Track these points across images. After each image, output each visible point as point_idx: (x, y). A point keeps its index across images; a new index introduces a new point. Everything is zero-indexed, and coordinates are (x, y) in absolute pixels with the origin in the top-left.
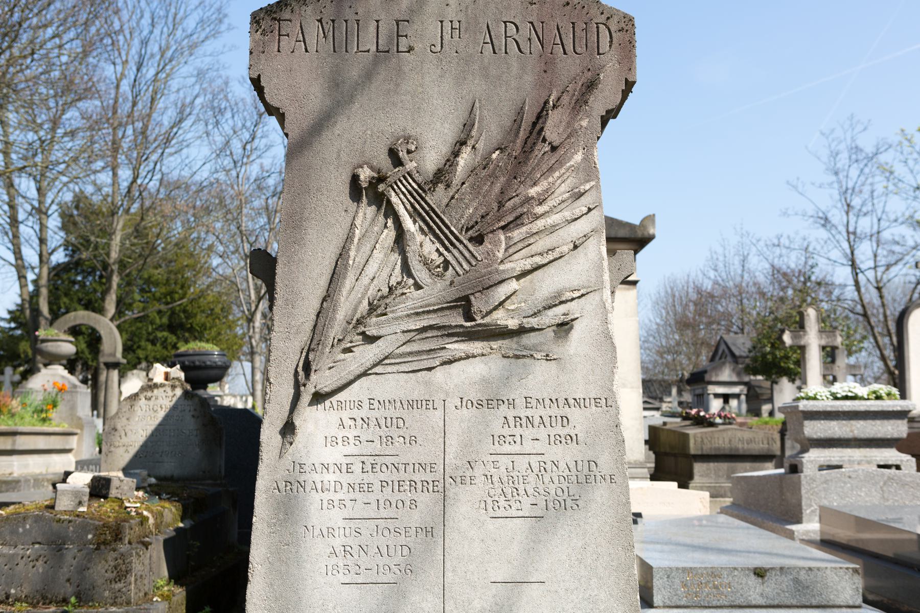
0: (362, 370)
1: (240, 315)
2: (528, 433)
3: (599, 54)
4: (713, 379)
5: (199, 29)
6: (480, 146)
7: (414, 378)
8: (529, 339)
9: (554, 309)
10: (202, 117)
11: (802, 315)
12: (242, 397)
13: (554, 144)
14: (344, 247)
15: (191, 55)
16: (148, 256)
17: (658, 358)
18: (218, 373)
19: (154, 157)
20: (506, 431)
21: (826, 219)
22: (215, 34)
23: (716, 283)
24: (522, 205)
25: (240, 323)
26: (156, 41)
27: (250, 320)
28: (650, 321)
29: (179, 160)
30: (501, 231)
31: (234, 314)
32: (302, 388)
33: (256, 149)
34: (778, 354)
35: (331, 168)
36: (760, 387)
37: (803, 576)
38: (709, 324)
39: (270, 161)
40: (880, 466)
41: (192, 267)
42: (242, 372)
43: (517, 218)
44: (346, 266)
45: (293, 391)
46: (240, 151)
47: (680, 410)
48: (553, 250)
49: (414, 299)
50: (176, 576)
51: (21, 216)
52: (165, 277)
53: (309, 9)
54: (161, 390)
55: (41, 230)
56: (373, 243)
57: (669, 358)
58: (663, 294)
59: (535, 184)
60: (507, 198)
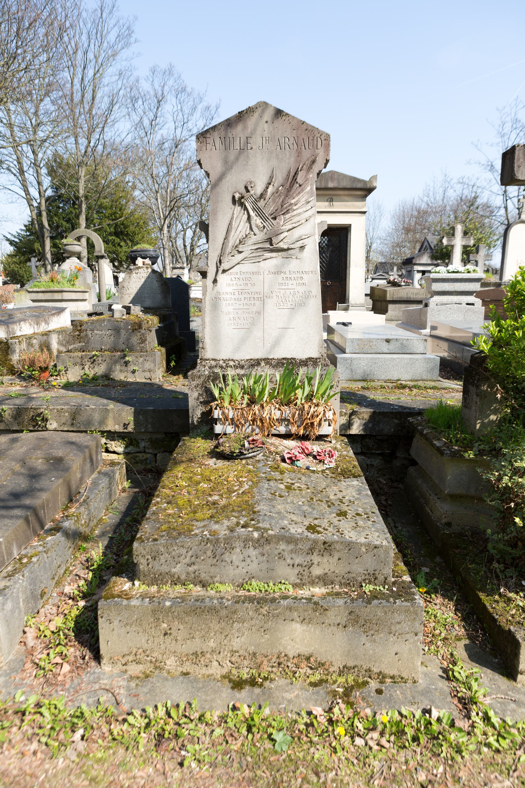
2: (290, 282)
4: (417, 262)
8: (290, 252)
11: (453, 229)
20: (283, 282)
21: (492, 166)
22: (127, 45)
27: (161, 230)
37: (404, 342)
39: (166, 131)
40: (467, 304)
41: (125, 197)
44: (231, 228)
49: (254, 239)
50: (161, 343)
51: (25, 169)
55: (38, 176)
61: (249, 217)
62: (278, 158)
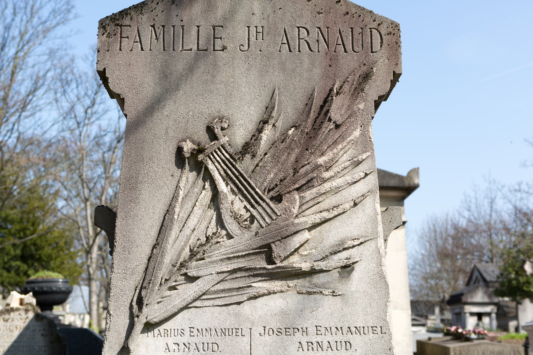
0: (184, 304)
1: (80, 247)
3: (372, 52)
4: (469, 300)
5: (51, 17)
6: (279, 124)
7: (226, 311)
9: (339, 254)
10: (52, 86)
12: (80, 315)
13: (338, 123)
14: (170, 205)
15: (45, 37)
16: (6, 199)
17: (423, 283)
18: (61, 297)
19: (13, 119)
22: (64, 21)
23: (469, 221)
24: (312, 171)
25: (80, 254)
26: (16, 27)
27: (88, 252)
28: (417, 252)
29: (33, 122)
30: (296, 192)
31: (75, 247)
32: (136, 319)
33: (95, 113)
34: (522, 280)
35: (161, 142)
36: (507, 307)
38: (465, 255)
41: (42, 208)
42: (80, 294)
43: (309, 181)
44: (172, 220)
45: (128, 321)
46: (82, 114)
47: (441, 326)
48: (337, 207)
49: (226, 246)
52: (20, 216)
53: (145, 17)
54: (17, 313)
56: (194, 201)
57: (433, 282)
58: (426, 230)
59: (323, 154)
60: (301, 165)
61: (216, 198)
62: (284, 70)
